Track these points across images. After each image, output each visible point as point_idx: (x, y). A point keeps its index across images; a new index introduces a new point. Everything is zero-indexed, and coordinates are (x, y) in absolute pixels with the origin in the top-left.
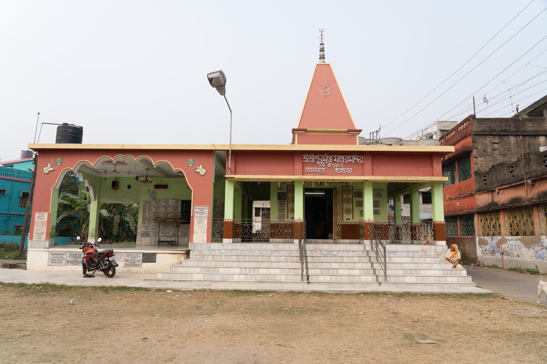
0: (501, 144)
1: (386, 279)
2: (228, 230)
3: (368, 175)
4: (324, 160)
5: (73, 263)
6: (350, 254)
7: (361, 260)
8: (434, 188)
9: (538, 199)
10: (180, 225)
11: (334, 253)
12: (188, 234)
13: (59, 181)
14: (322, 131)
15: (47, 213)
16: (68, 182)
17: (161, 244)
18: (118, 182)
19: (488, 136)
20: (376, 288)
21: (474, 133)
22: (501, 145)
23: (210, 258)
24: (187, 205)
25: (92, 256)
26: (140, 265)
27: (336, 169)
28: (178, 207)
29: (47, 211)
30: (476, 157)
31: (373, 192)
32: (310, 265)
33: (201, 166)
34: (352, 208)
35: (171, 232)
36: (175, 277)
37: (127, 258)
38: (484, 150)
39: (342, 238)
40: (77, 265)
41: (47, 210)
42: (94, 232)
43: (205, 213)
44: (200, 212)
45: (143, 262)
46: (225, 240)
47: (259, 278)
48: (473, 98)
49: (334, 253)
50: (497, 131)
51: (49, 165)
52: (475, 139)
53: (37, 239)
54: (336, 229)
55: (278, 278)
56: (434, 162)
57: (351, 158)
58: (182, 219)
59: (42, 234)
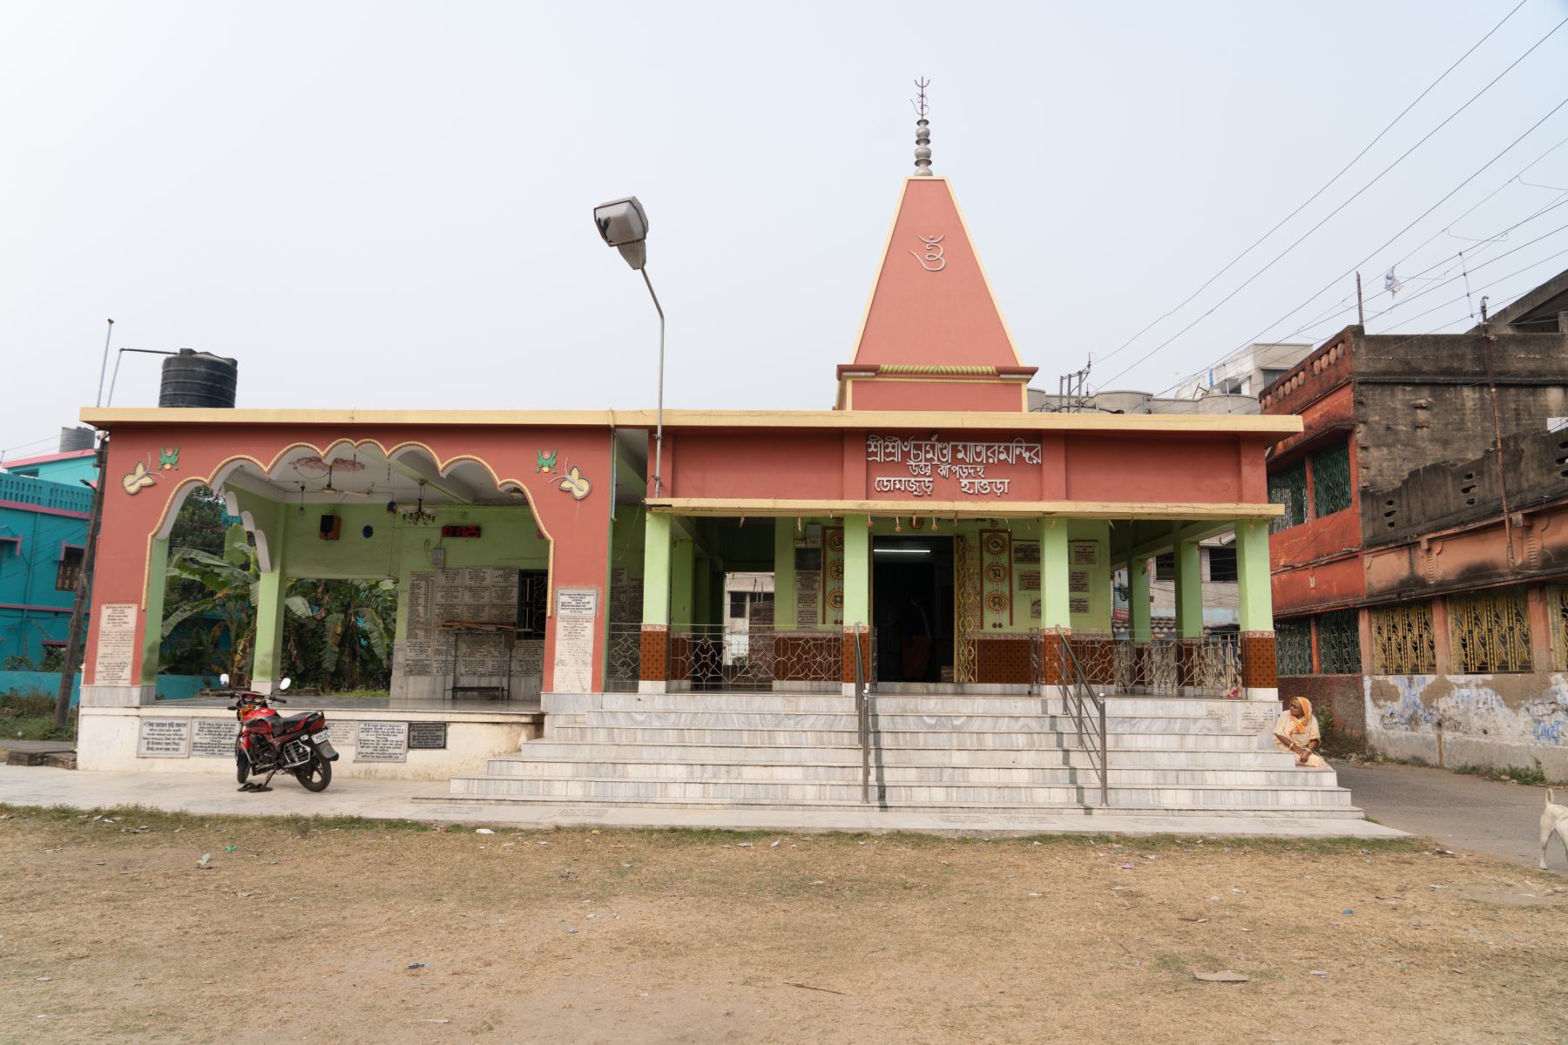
0: (1435, 410)
1: (1105, 798)
2: (653, 656)
3: (1055, 498)
4: (929, 456)
5: (210, 749)
6: (1004, 725)
10: (516, 642)
11: (957, 722)
12: (539, 668)
13: (168, 514)
14: (911, 373)
15: (134, 608)
16: (196, 517)
17: (461, 695)
18: (339, 519)
21: (1359, 379)
23: (602, 736)
24: (537, 585)
25: (263, 730)
27: (964, 482)
28: (509, 589)
30: (1365, 448)
31: (1069, 546)
32: (887, 757)
33: (575, 473)
36: (502, 790)
37: (363, 736)
38: (1388, 428)
39: (980, 681)
42: (270, 661)
43: (588, 606)
44: (574, 603)
45: (409, 747)
46: (644, 685)
47: (743, 793)
49: (957, 722)
51: (140, 470)
52: (1361, 395)
54: (962, 653)
55: (795, 794)
56: (1244, 461)
57: (1007, 449)
58: (521, 624)
59: (122, 666)
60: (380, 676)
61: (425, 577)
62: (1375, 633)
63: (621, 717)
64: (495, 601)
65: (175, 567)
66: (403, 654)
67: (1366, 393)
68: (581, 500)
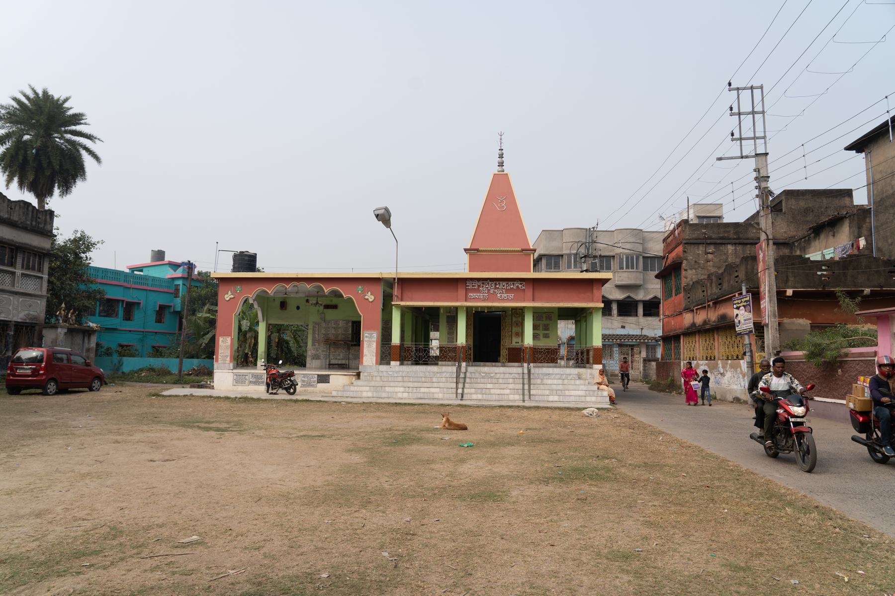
0: (716, 254)
1: (530, 398)
3: (529, 301)
4: (487, 286)
5: (256, 383)
6: (507, 376)
7: (515, 381)
8: (594, 317)
9: (718, 322)
10: (351, 347)
11: (492, 375)
12: (358, 357)
14: (494, 251)
15: (230, 337)
17: (331, 366)
18: (286, 302)
19: (702, 245)
20: (521, 404)
21: (684, 241)
22: (716, 256)
23: (378, 378)
25: (275, 376)
26: (315, 386)
27: (499, 295)
29: (229, 336)
33: (369, 293)
34: (521, 331)
35: (342, 355)
36: (348, 394)
37: (303, 379)
38: (696, 262)
39: (509, 362)
40: (259, 385)
41: (230, 335)
42: (263, 354)
45: (318, 382)
46: (393, 363)
47: (420, 396)
48: (687, 199)
49: (492, 375)
50: (713, 239)
51: (230, 293)
53: (222, 362)
54: (504, 352)
55: (436, 396)
56: (594, 288)
57: (513, 284)
58: (352, 341)
59: (226, 356)
60: (291, 360)
61: (318, 324)
62: (704, 343)
63: (384, 373)
64: (343, 332)
65: (206, 313)
66: (310, 351)
67: (687, 247)
68: (371, 302)
